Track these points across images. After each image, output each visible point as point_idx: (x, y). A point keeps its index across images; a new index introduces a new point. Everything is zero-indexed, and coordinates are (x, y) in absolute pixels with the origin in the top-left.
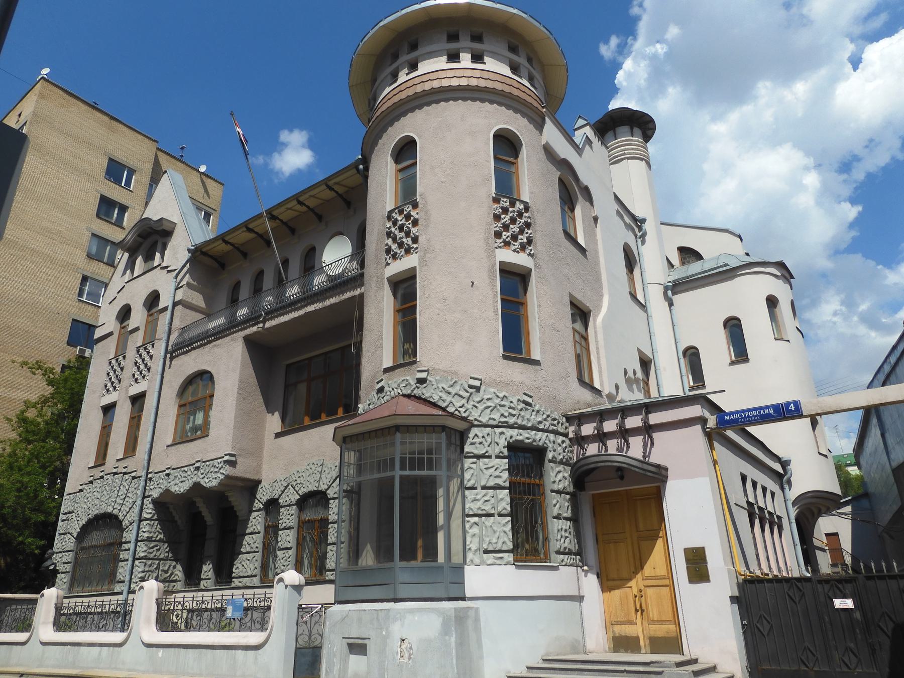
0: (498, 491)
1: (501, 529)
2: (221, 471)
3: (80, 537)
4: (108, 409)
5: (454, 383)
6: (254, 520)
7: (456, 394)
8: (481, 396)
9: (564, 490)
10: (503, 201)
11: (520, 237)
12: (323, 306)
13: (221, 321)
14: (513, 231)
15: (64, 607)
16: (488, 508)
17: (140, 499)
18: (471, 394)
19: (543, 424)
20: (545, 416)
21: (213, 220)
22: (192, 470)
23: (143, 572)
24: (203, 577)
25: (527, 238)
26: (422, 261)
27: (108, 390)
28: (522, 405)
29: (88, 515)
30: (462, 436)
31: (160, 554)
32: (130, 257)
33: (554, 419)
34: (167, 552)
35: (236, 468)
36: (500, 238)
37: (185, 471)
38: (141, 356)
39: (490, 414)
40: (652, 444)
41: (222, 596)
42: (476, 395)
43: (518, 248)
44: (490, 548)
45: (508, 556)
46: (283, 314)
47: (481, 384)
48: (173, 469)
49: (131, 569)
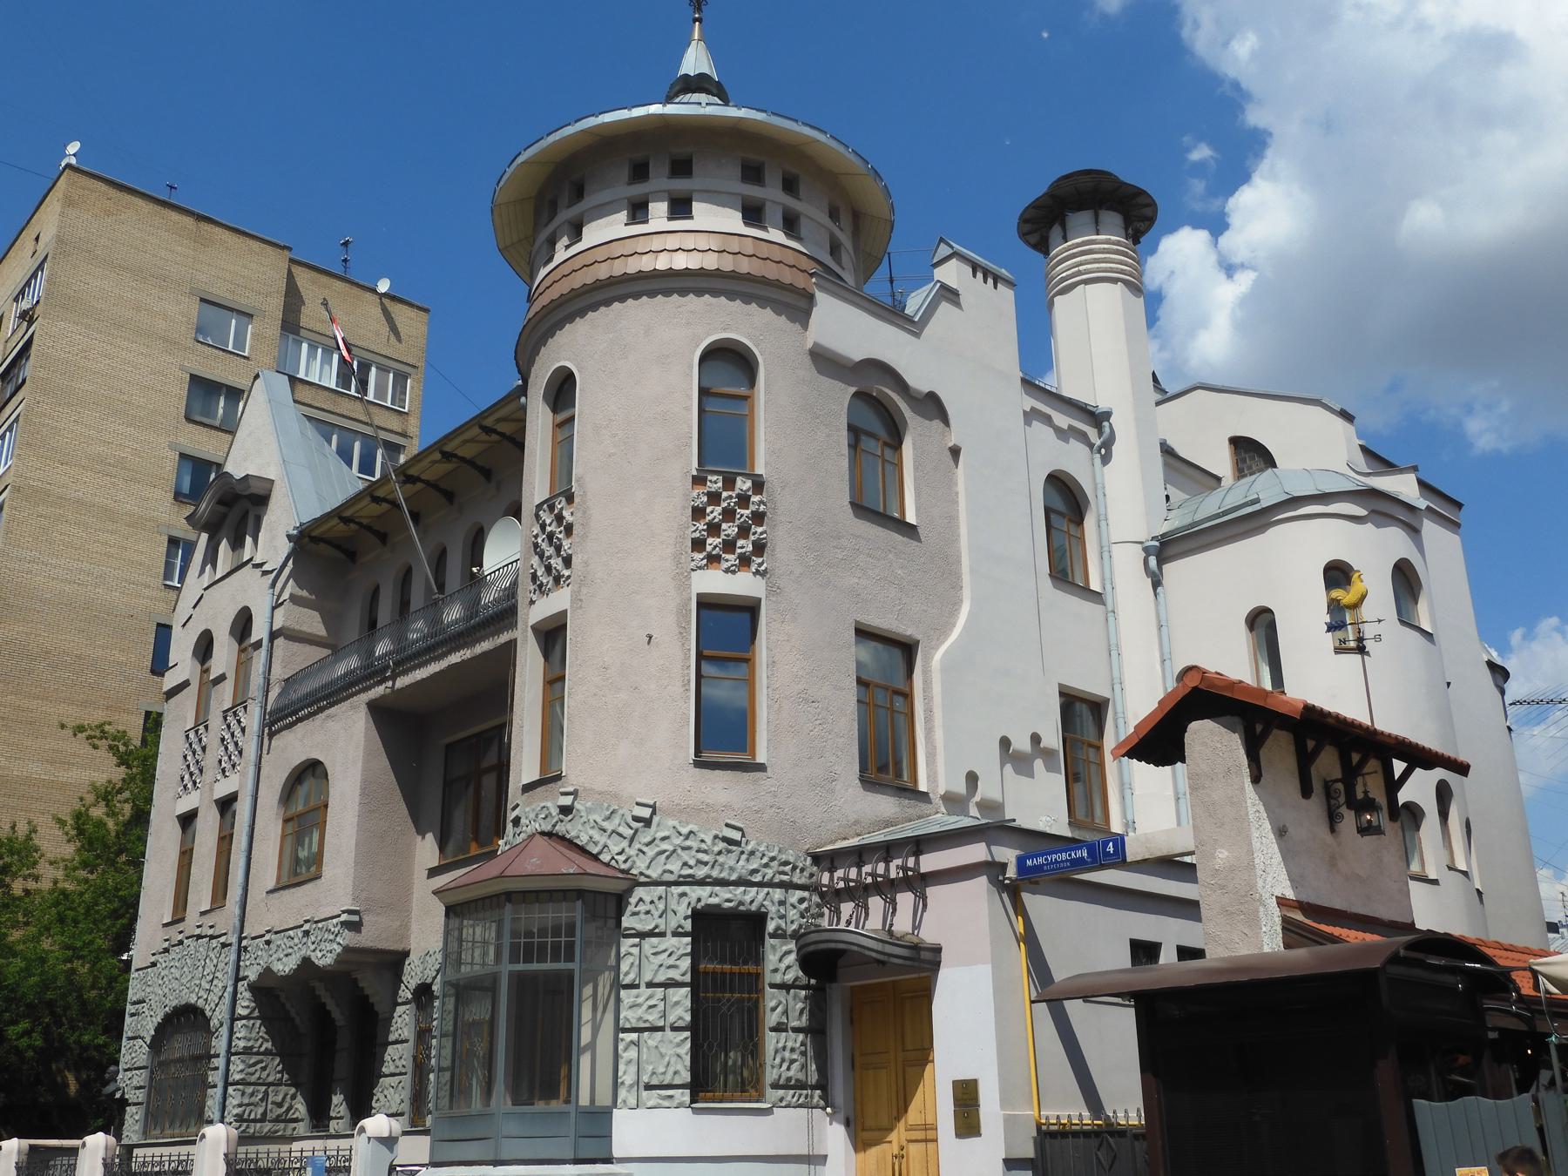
0: (671, 991)
1: (671, 1052)
2: (338, 939)
3: (156, 1044)
4: (187, 820)
5: (612, 813)
6: (399, 1020)
7: (613, 832)
8: (652, 834)
9: (797, 983)
10: (711, 481)
11: (740, 543)
12: (473, 656)
13: (352, 662)
14: (725, 535)
15: (240, 1159)
16: (653, 1018)
17: (231, 983)
18: (636, 831)
19: (760, 873)
20: (765, 860)
21: (412, 388)
22: (300, 935)
23: (240, 1105)
24: (333, 1114)
25: (754, 543)
26: (576, 599)
27: (185, 786)
28: (721, 845)
29: (165, 1007)
30: (620, 901)
31: (268, 1075)
32: (210, 539)
33: (786, 863)
34: (279, 1072)
35: (361, 932)
36: (700, 552)
37: (290, 937)
38: (229, 726)
39: (665, 864)
40: (925, 906)
41: (302, 1151)
42: (644, 832)
43: (732, 566)
44: (655, 1082)
45: (682, 1093)
46: (419, 666)
47: (654, 813)
48: (276, 933)
49: (221, 1100)
